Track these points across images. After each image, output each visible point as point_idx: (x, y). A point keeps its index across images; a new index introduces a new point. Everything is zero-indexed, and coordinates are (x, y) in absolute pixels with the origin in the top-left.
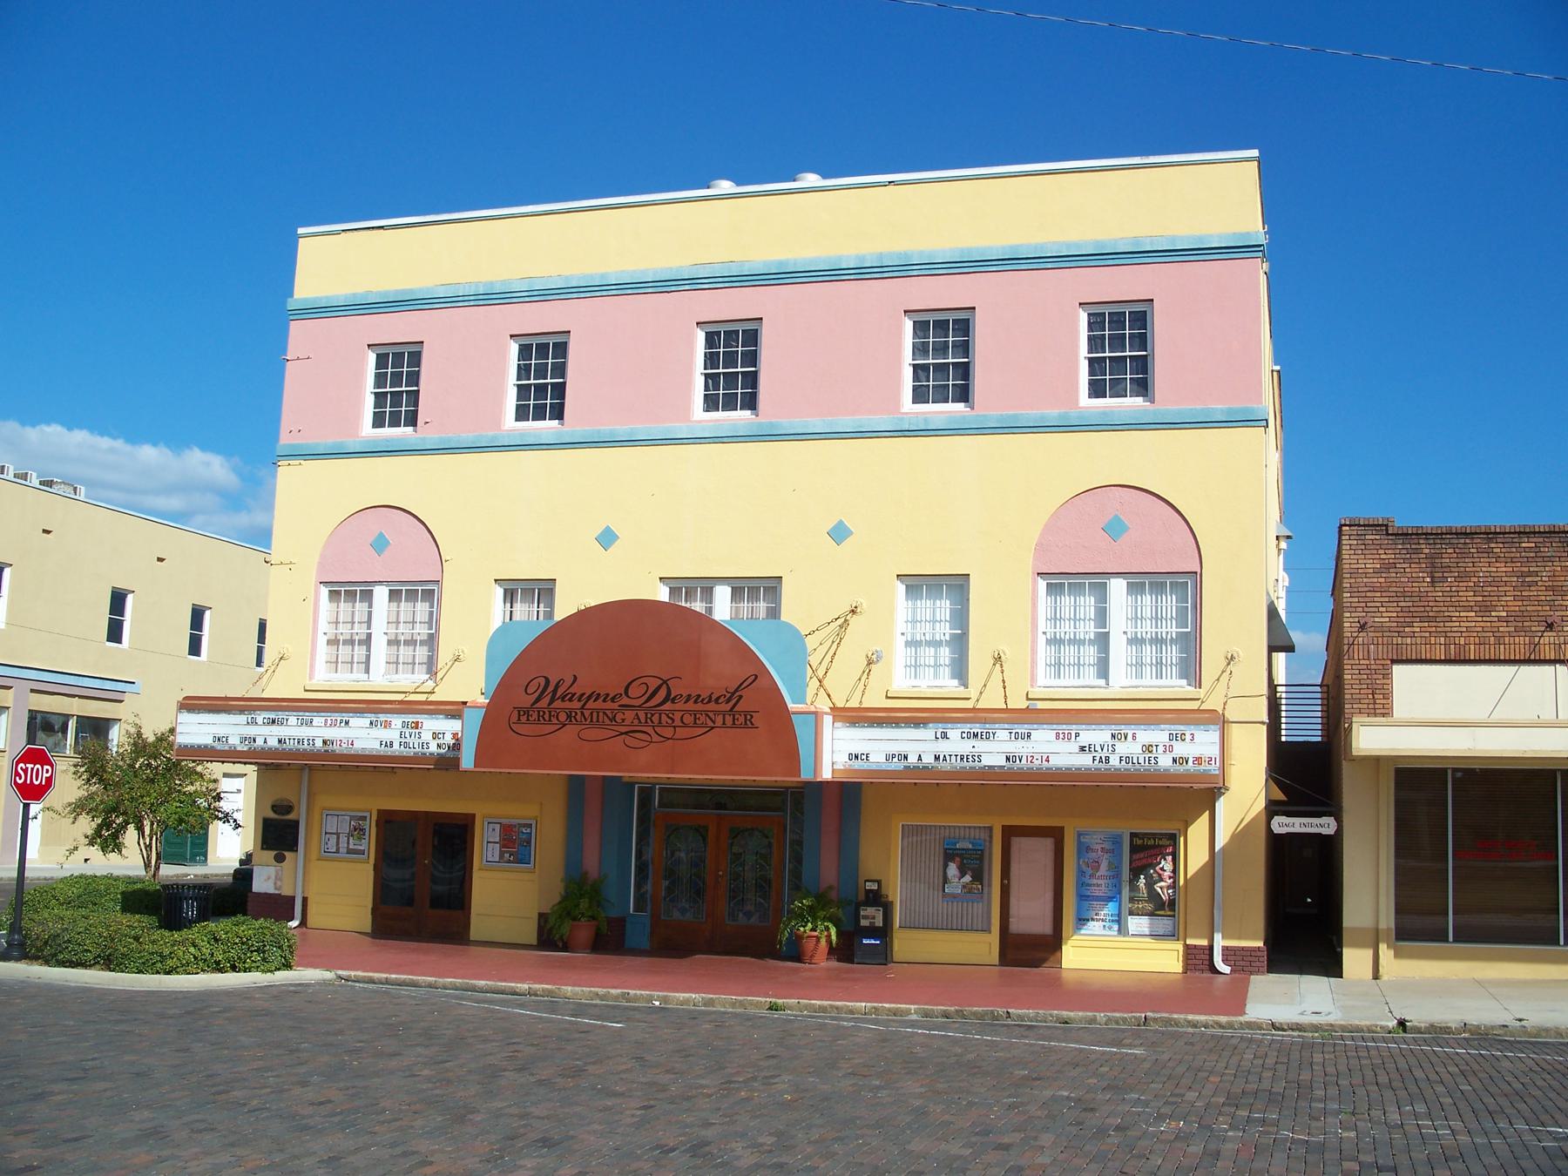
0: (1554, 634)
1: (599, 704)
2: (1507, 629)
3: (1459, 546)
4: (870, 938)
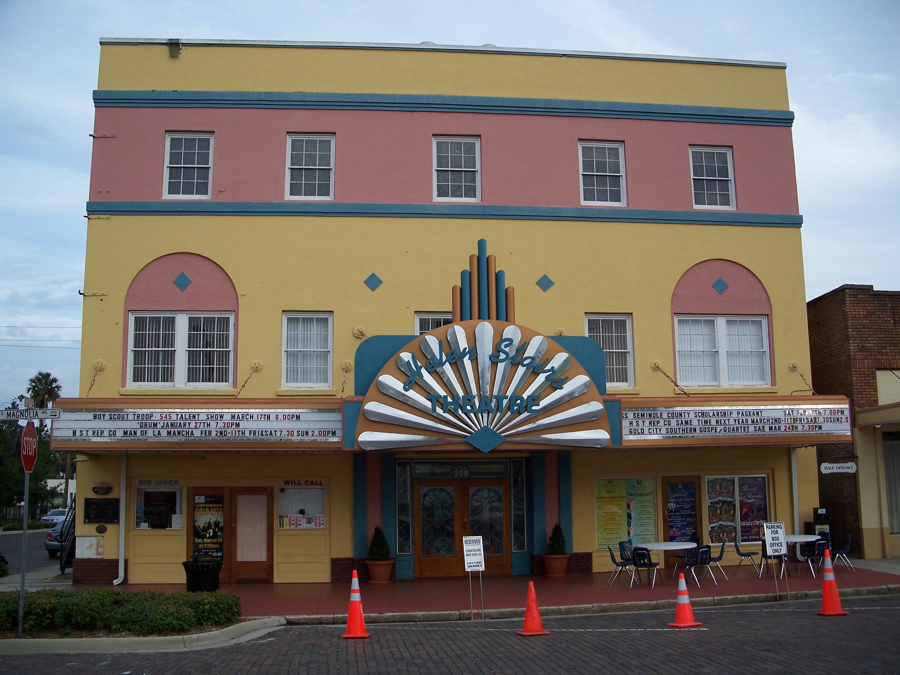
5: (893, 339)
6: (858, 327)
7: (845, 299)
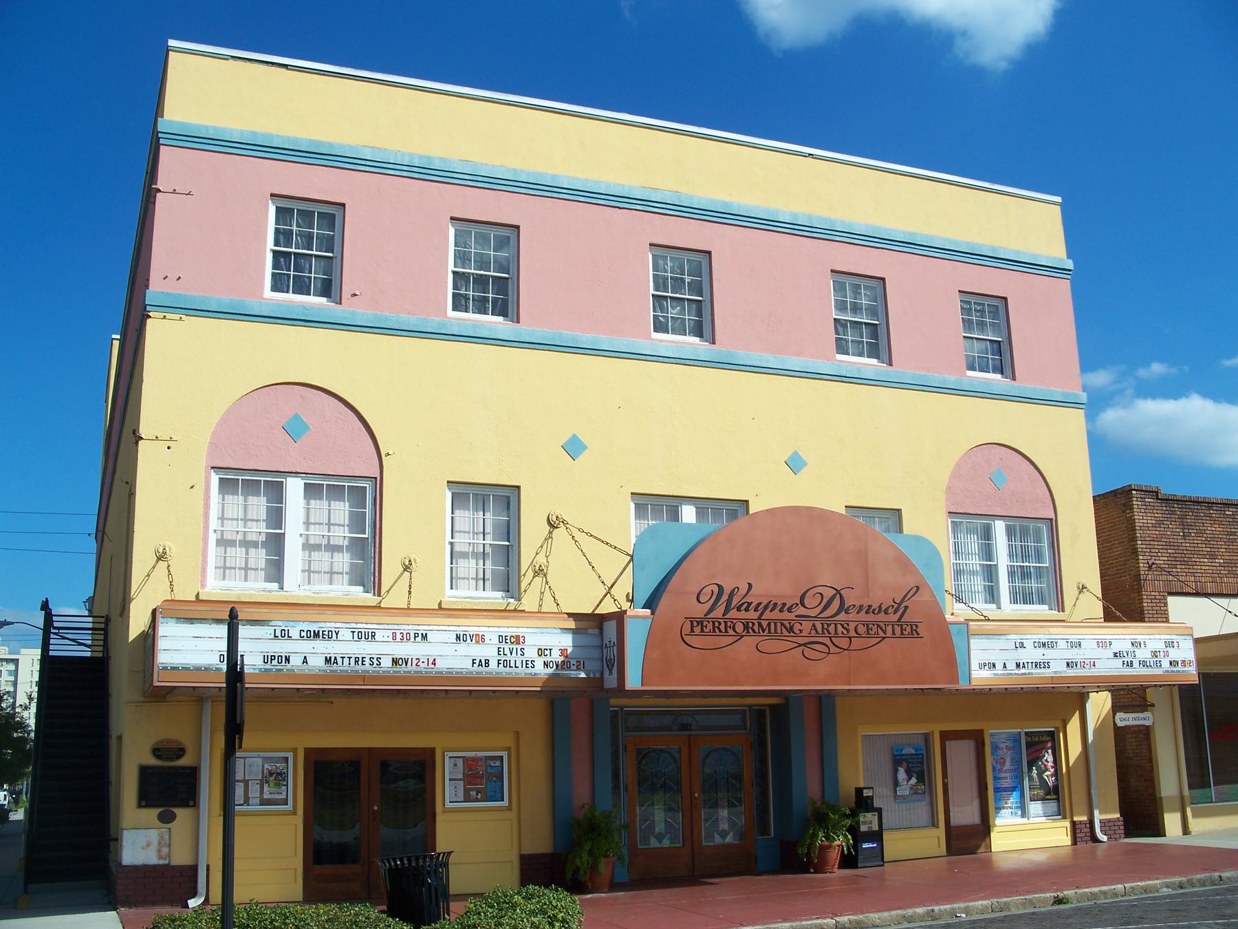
2: (1225, 572)
3: (1195, 511)
5: (1183, 555)
6: (1147, 539)
7: (1131, 503)
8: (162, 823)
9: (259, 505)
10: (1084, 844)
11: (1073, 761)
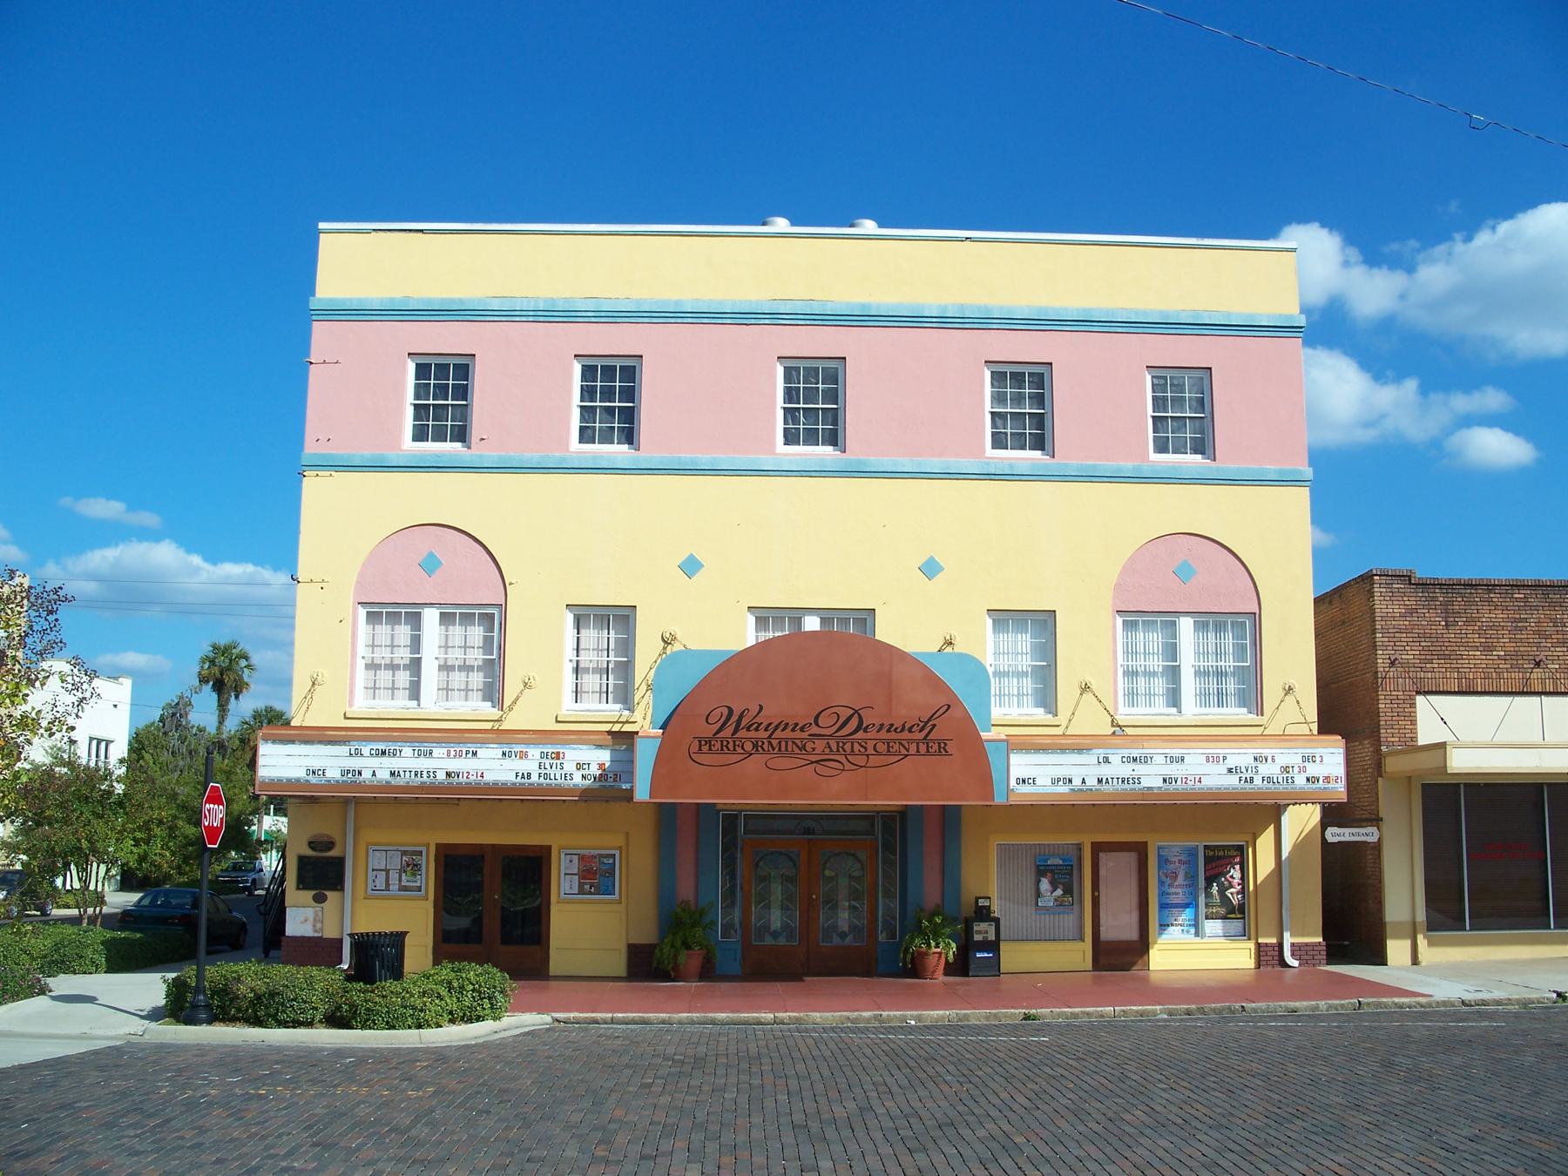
0: (1542, 670)
1: (788, 734)
2: (1506, 666)
4: (983, 951)
5: (1444, 648)
8: (316, 902)
9: (403, 632)
10: (1269, 968)
11: (1262, 878)
